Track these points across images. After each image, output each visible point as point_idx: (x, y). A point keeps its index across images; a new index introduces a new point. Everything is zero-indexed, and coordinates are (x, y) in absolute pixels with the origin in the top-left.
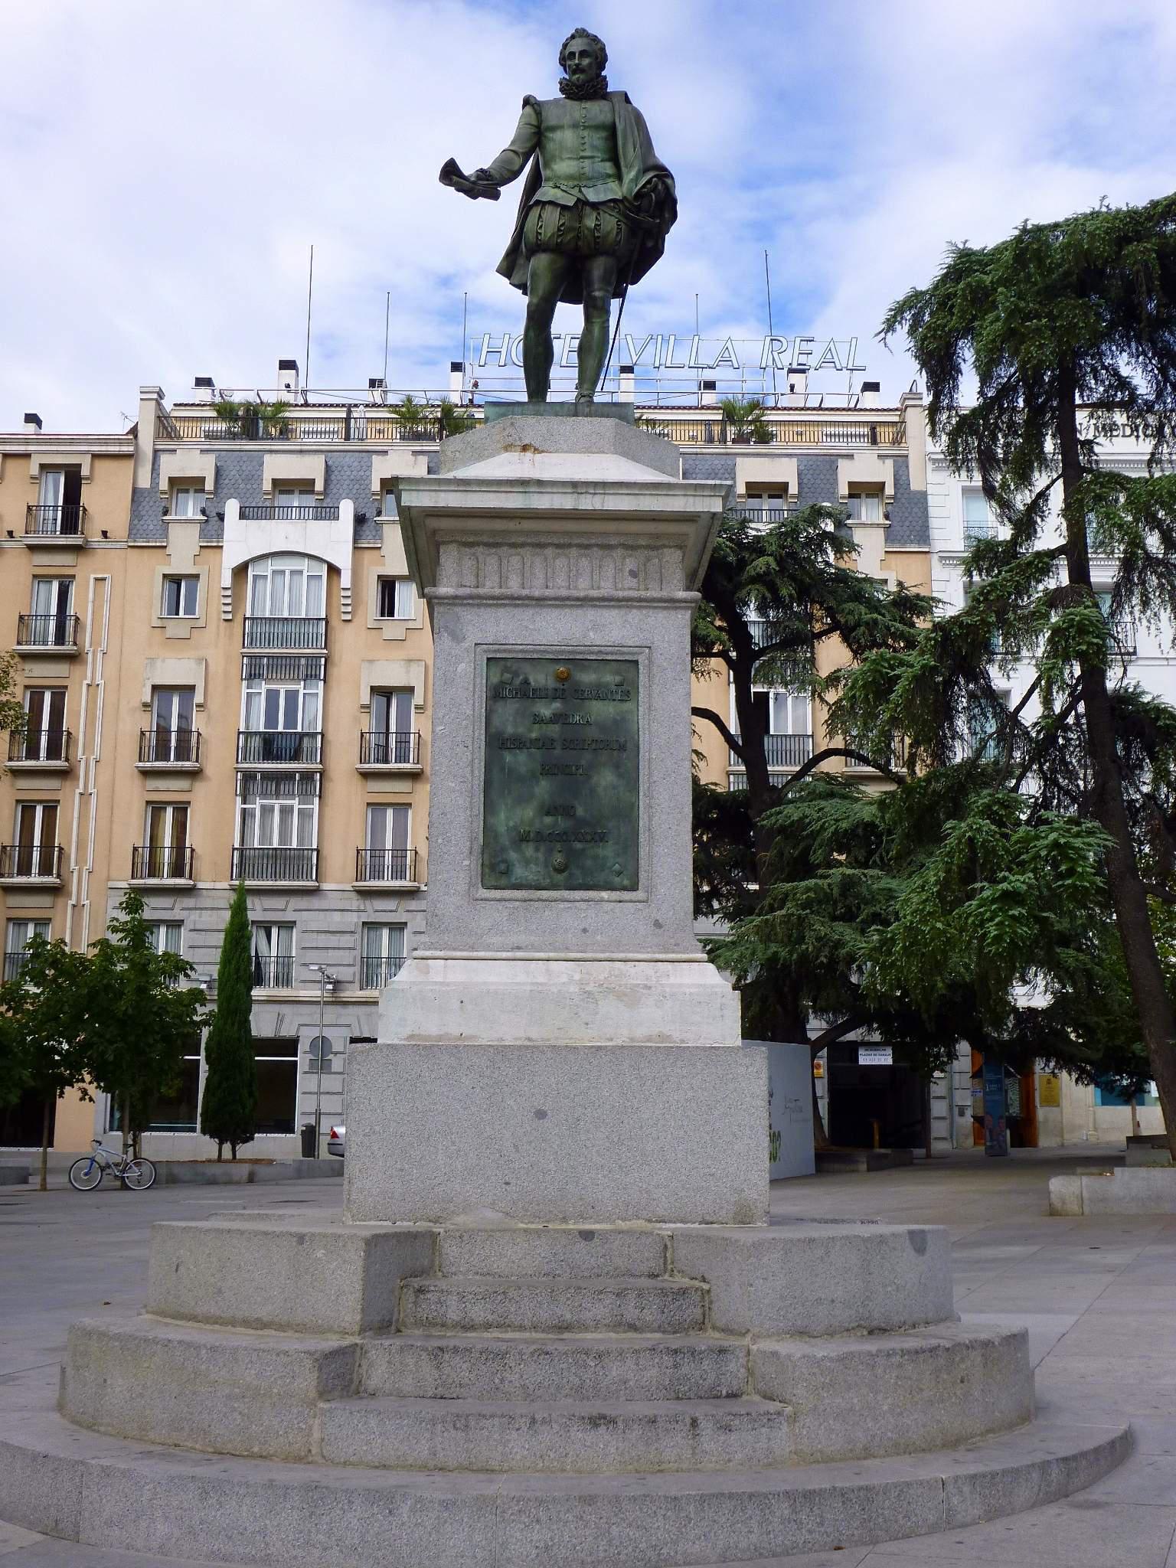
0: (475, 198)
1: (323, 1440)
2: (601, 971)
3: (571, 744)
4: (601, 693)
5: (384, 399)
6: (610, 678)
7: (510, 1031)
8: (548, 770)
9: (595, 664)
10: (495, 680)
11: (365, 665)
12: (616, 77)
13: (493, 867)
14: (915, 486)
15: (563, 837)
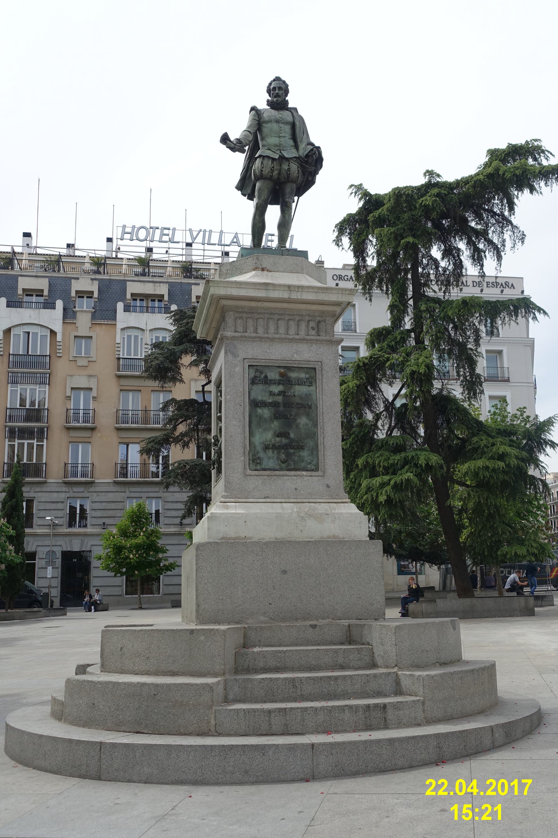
0: (234, 151)
1: (216, 724)
2: (306, 507)
3: (288, 404)
4: (300, 382)
5: (74, 253)
6: (303, 375)
7: (268, 533)
8: (277, 416)
9: (297, 369)
10: (252, 375)
11: (68, 378)
12: (292, 100)
13: (253, 461)
15: (285, 447)
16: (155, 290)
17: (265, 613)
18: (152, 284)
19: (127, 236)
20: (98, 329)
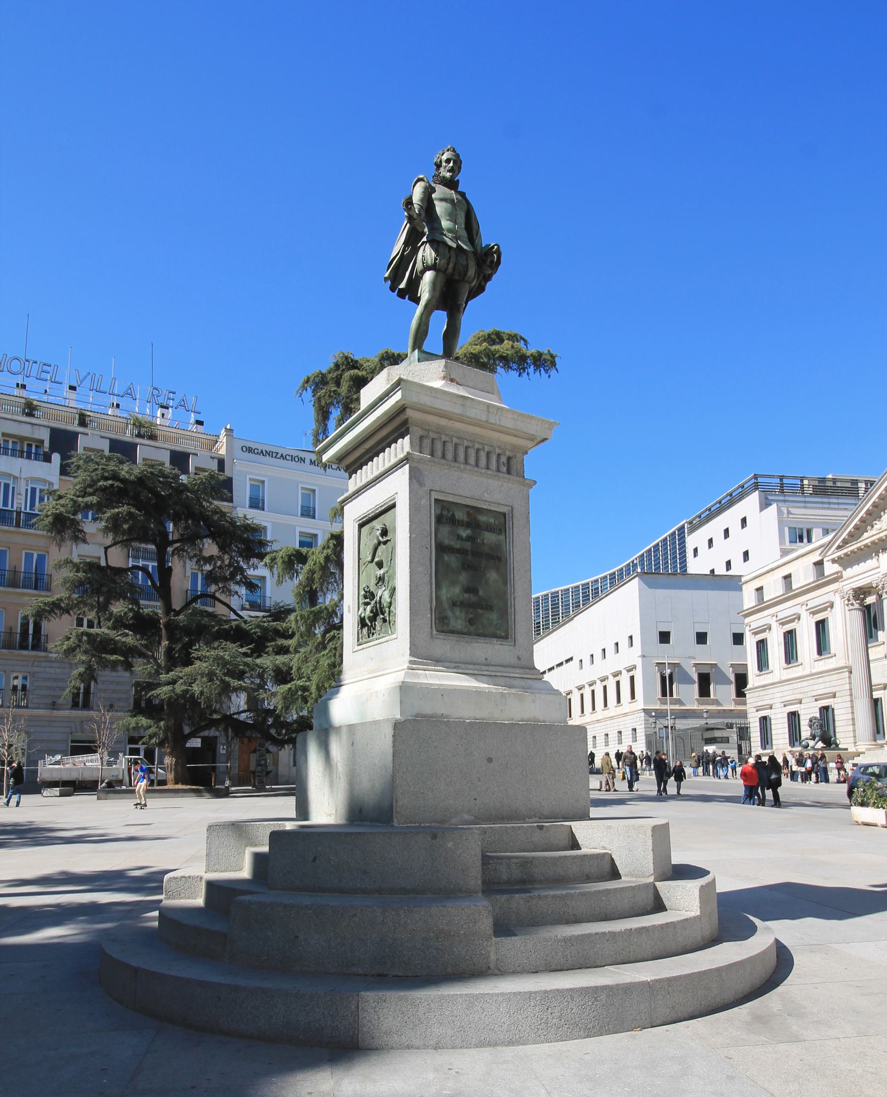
3: (477, 554)
4: (490, 529)
7: (467, 712)
8: (466, 566)
10: (438, 512)
16: (33, 433)
17: (470, 811)
18: (29, 426)
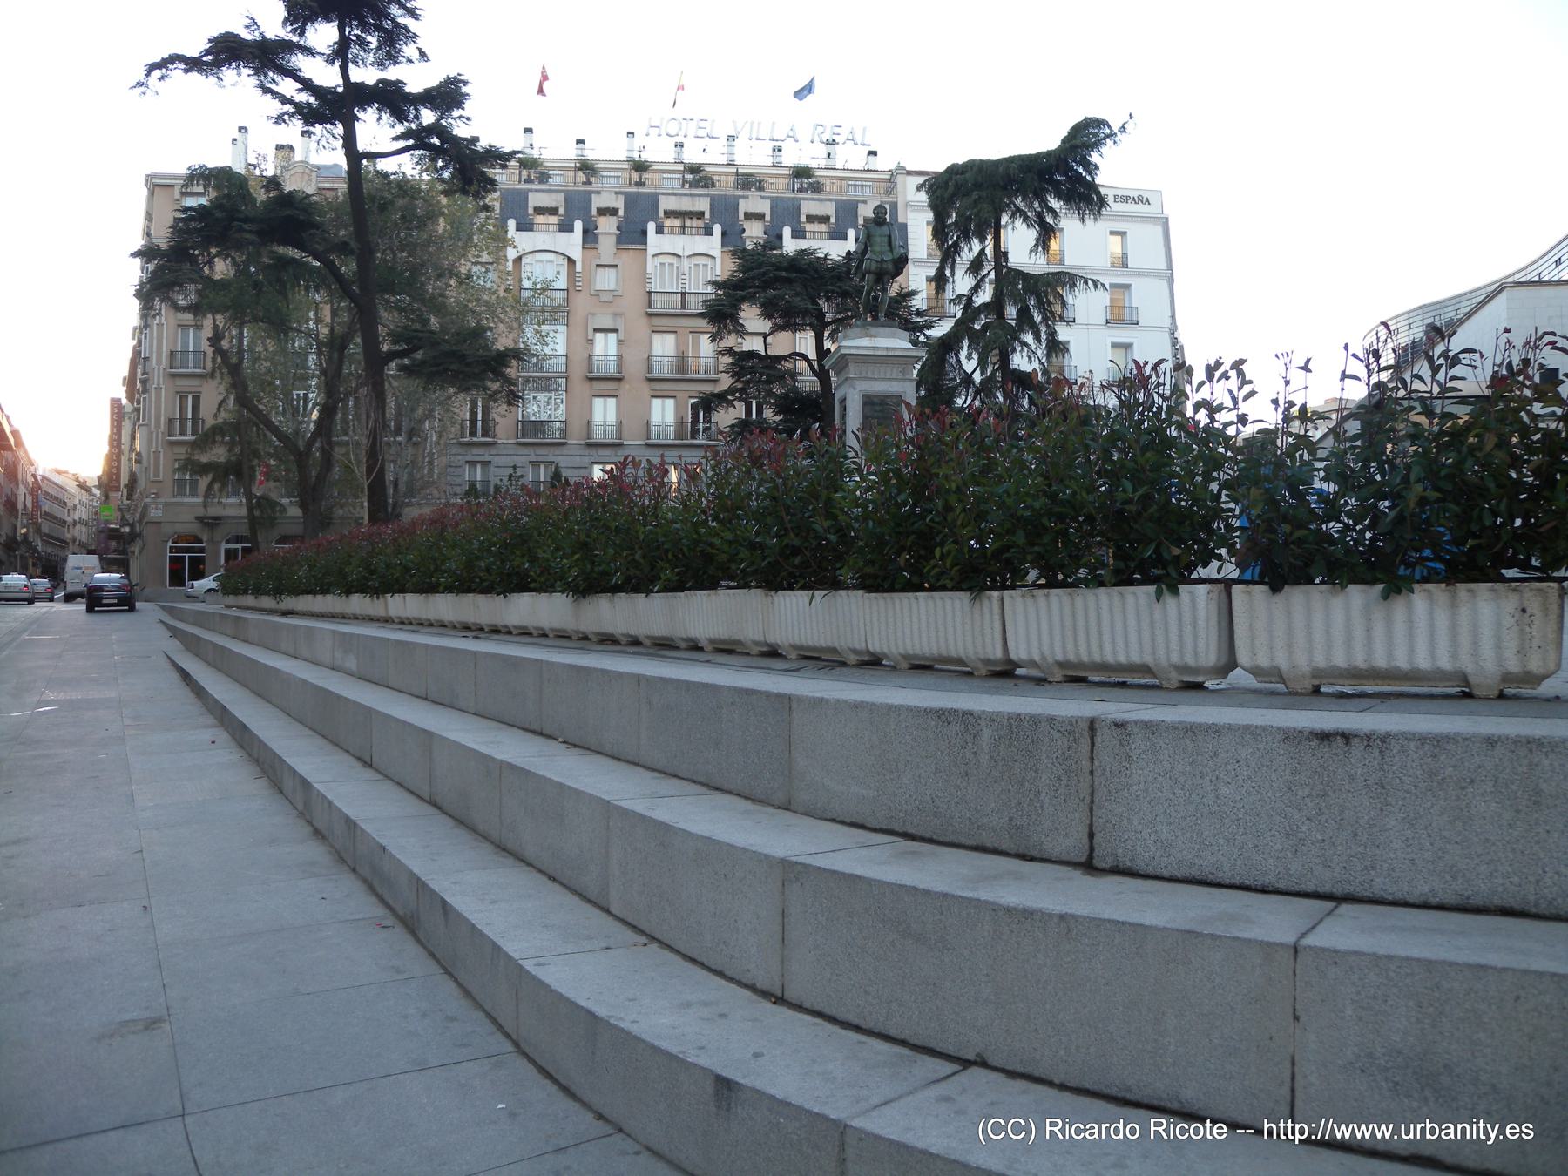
14: (900, 220)
19: (654, 132)
20: (624, 255)
